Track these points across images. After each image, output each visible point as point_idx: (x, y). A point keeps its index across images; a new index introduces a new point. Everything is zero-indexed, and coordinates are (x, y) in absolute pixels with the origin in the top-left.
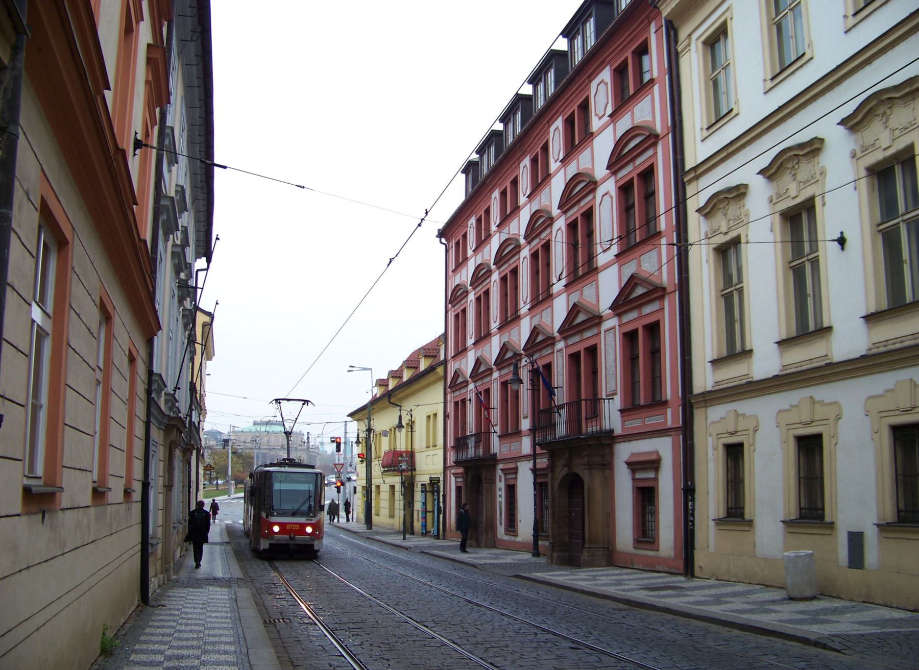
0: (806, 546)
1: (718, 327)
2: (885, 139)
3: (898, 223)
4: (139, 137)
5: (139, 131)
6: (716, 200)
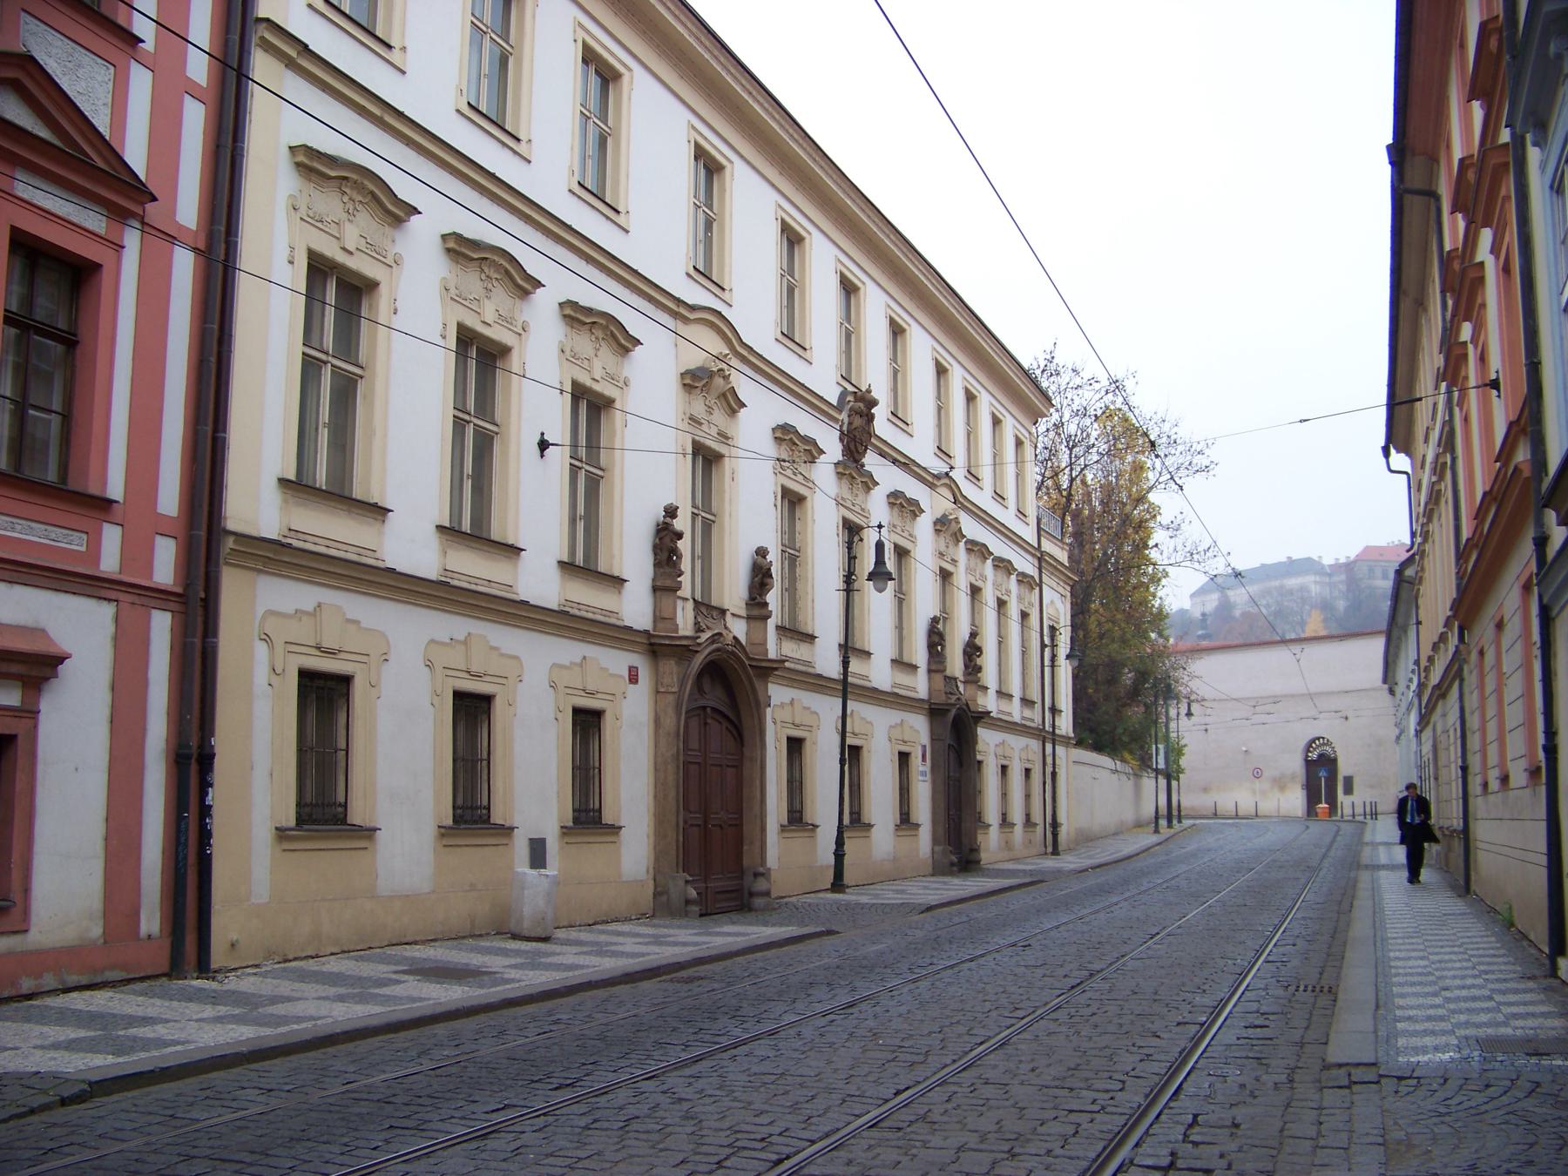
0: (475, 859)
1: (862, 610)
2: (351, 237)
3: (325, 363)
4: (1494, 392)
5: (1495, 400)
6: (354, 176)
